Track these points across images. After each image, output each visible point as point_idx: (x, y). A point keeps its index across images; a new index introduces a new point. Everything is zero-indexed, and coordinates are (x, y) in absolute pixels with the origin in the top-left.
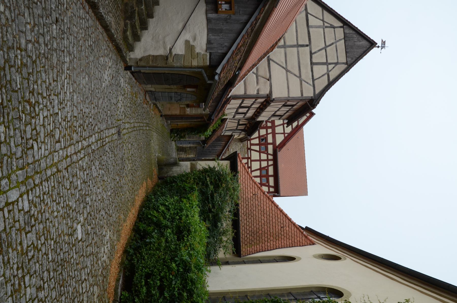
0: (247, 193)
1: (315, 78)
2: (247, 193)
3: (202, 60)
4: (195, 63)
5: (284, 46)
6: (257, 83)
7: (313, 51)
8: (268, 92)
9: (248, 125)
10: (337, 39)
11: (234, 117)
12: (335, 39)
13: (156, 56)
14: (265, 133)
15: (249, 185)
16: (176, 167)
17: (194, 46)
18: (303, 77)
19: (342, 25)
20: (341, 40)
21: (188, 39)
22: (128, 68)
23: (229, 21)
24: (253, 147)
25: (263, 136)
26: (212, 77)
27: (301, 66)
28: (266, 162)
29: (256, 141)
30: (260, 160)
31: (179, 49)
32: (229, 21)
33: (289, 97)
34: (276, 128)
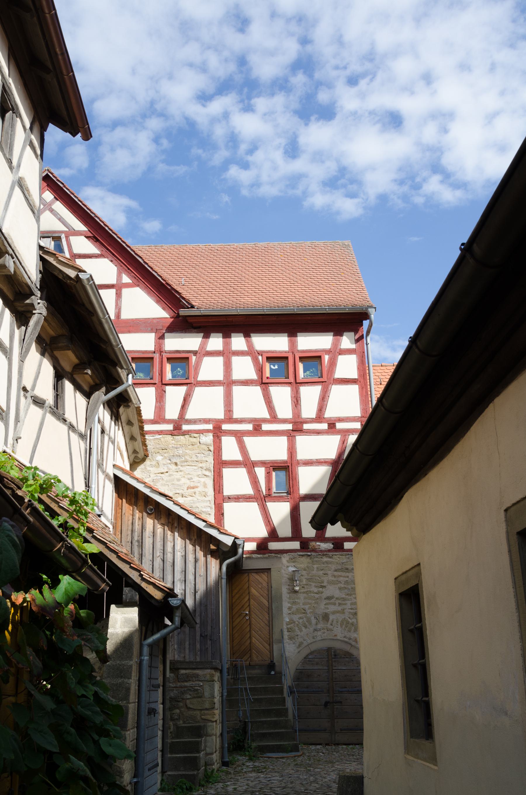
24: (172, 412)
28: (235, 360)
30: (228, 383)
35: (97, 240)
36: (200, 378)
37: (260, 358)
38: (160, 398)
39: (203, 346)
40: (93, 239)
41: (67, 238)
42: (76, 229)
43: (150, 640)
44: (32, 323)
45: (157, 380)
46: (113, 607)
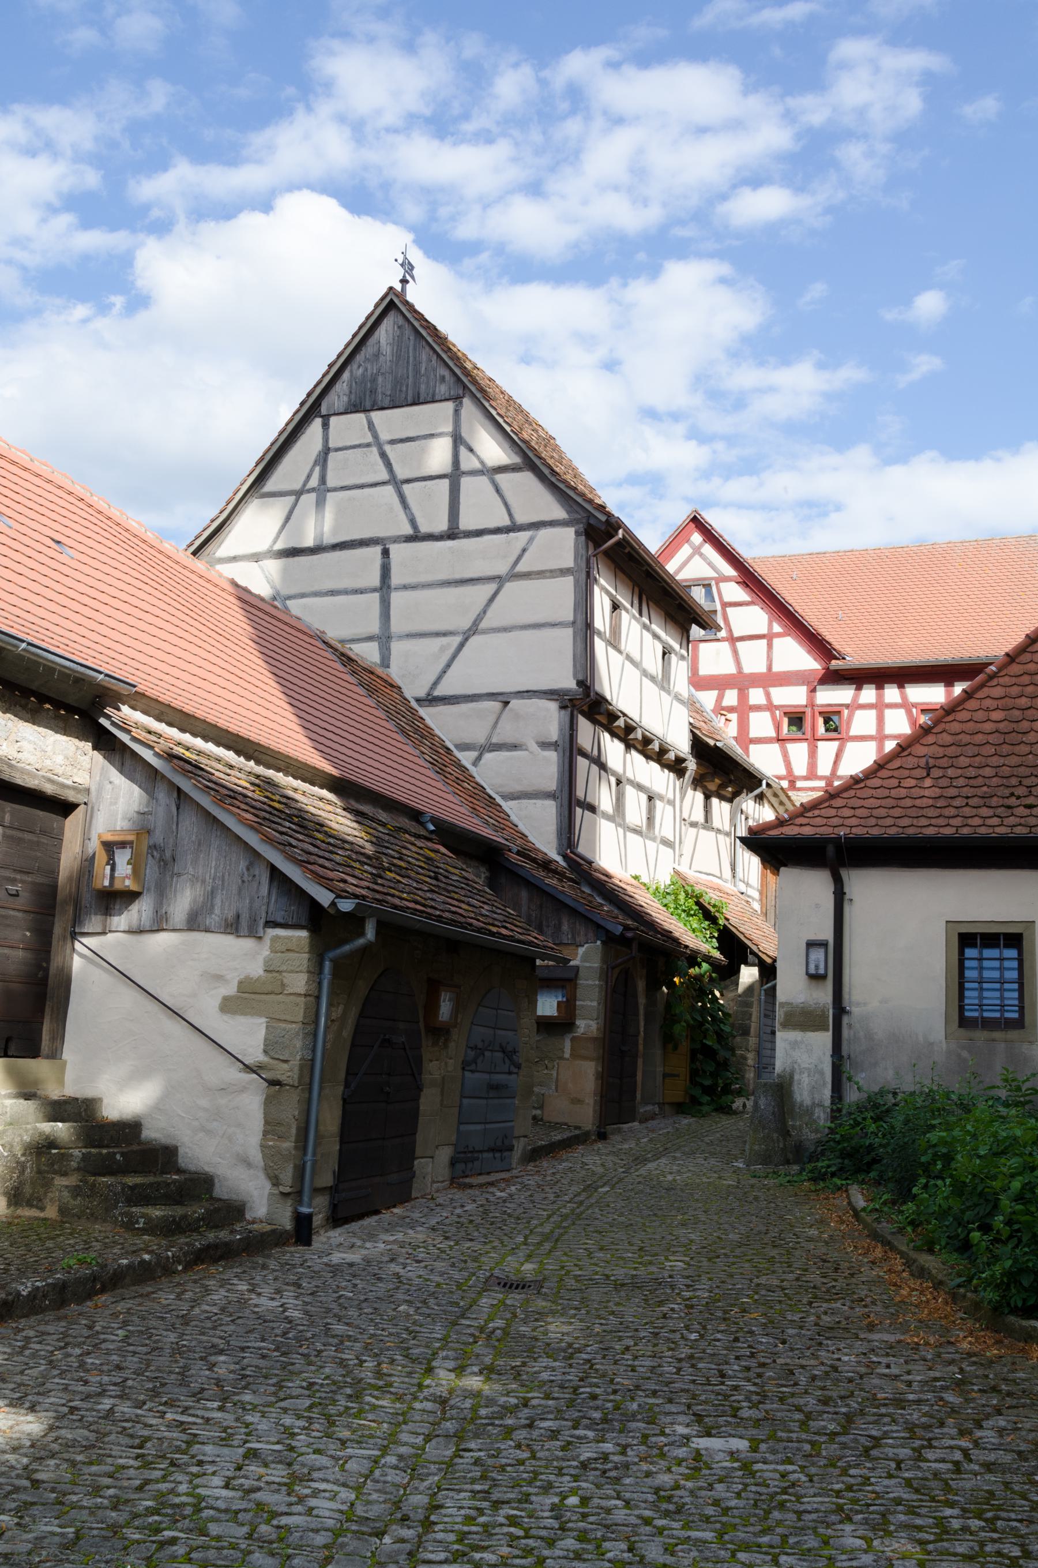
0: (918, 803)
1: (506, 522)
2: (918, 803)
3: (291, 955)
4: (299, 982)
5: (384, 639)
6: (515, 747)
7: (408, 531)
8: (553, 706)
9: (712, 786)
10: (369, 439)
11: (666, 843)
12: (368, 445)
13: (267, 1123)
14: (767, 715)
15: (886, 793)
16: (795, 1088)
17: (240, 983)
18: (502, 568)
19: (317, 422)
20: (371, 426)
21: (217, 1002)
22: (303, 1231)
23: (168, 854)
25: (778, 728)
26: (354, 921)
27: (458, 576)
28: (888, 712)
29: (799, 751)
31: (248, 1036)
32: (168, 854)
33: (574, 623)
34: (747, 669)
35: (748, 586)
36: (852, 733)
37: (914, 710)
38: (813, 754)
39: (855, 698)
40: (744, 584)
41: (717, 584)
42: (726, 574)
43: (765, 987)
44: (687, 776)
45: (809, 735)
46: (743, 966)
